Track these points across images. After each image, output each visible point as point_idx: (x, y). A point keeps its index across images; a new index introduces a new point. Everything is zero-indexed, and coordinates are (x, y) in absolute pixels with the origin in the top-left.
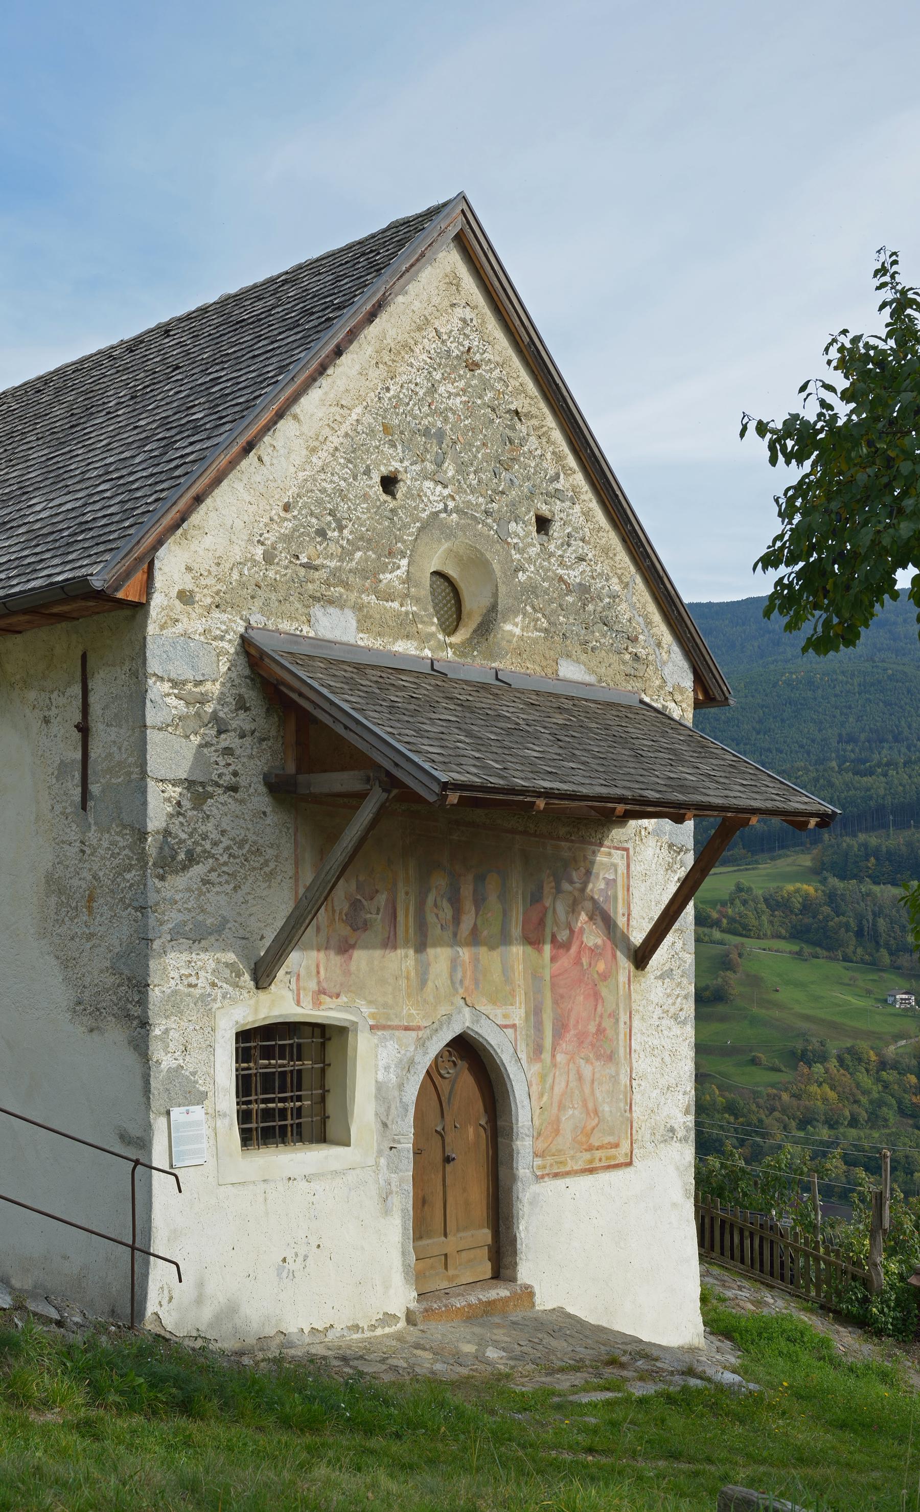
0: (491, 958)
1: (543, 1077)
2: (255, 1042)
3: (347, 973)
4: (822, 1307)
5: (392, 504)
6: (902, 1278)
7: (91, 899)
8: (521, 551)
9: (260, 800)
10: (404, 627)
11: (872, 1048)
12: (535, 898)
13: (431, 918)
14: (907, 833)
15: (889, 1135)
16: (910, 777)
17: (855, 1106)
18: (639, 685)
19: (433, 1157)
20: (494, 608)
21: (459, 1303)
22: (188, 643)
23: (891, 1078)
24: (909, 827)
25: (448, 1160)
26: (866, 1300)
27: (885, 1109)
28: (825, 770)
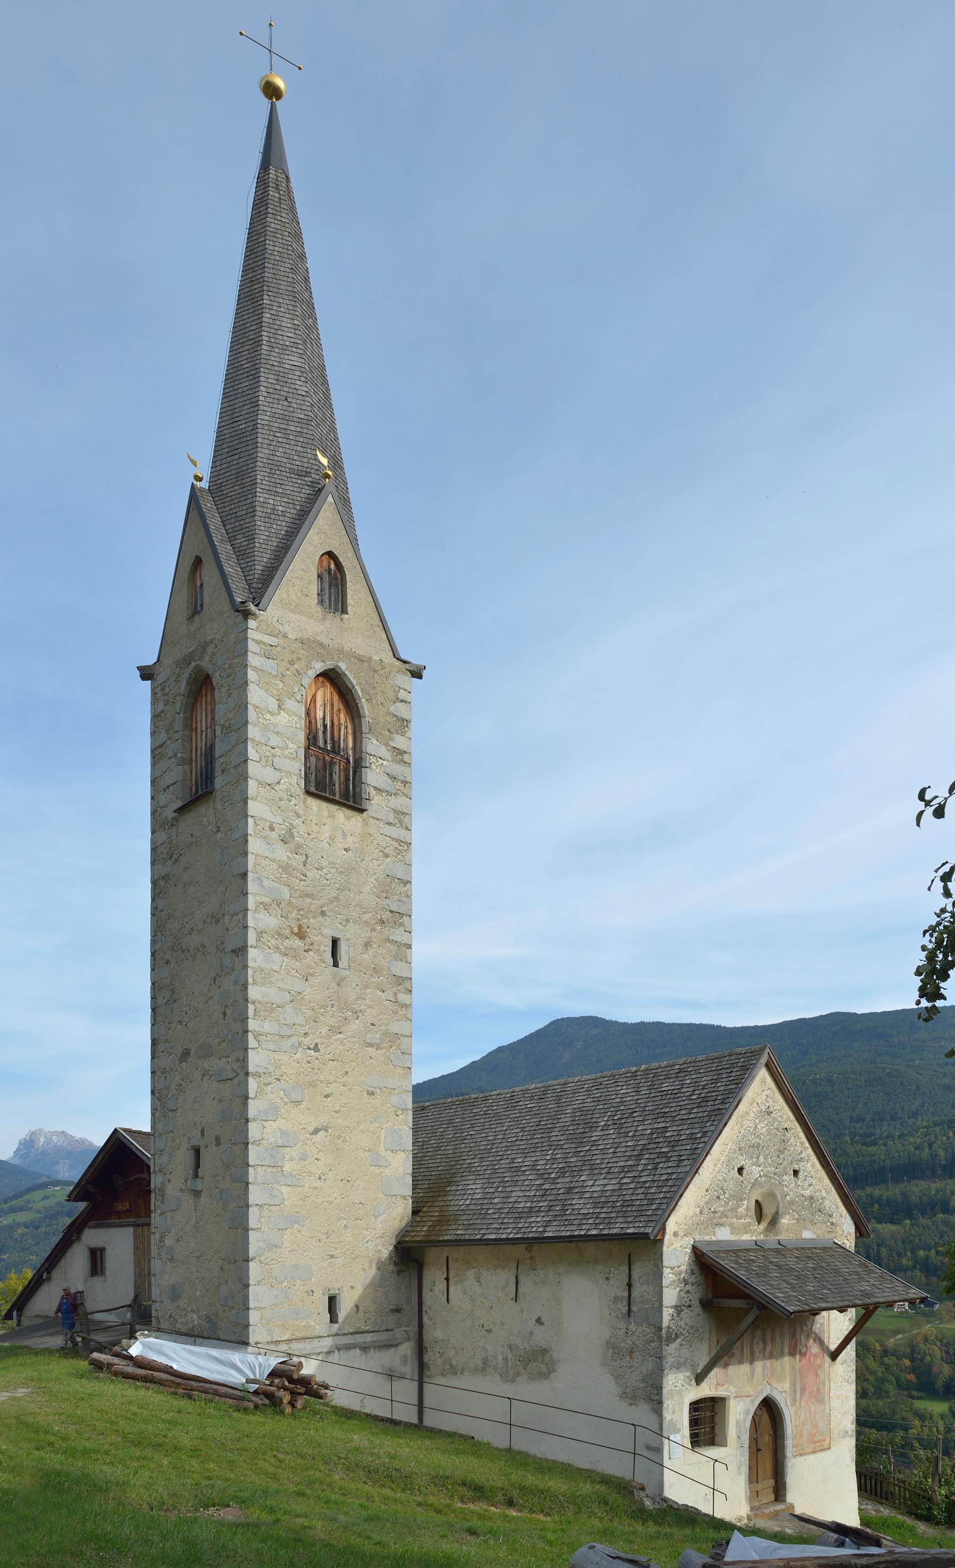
0: (777, 1363)
1: (796, 1413)
2: (696, 1406)
3: (727, 1375)
4: (908, 1512)
5: (742, 1178)
6: (946, 1497)
7: (631, 1352)
8: (788, 1187)
9: (698, 1309)
10: (746, 1229)
11: (877, 1341)
12: (793, 1335)
13: (756, 1349)
14: (902, 1186)
15: (890, 1403)
16: (903, 1145)
17: (865, 1383)
18: (833, 1235)
19: (755, 1449)
20: (777, 1213)
21: (767, 1511)
22: (676, 1253)
23: (891, 1363)
24: (903, 1181)
25: (758, 1450)
26: (930, 1508)
27: (887, 1385)
28: (841, 1143)
